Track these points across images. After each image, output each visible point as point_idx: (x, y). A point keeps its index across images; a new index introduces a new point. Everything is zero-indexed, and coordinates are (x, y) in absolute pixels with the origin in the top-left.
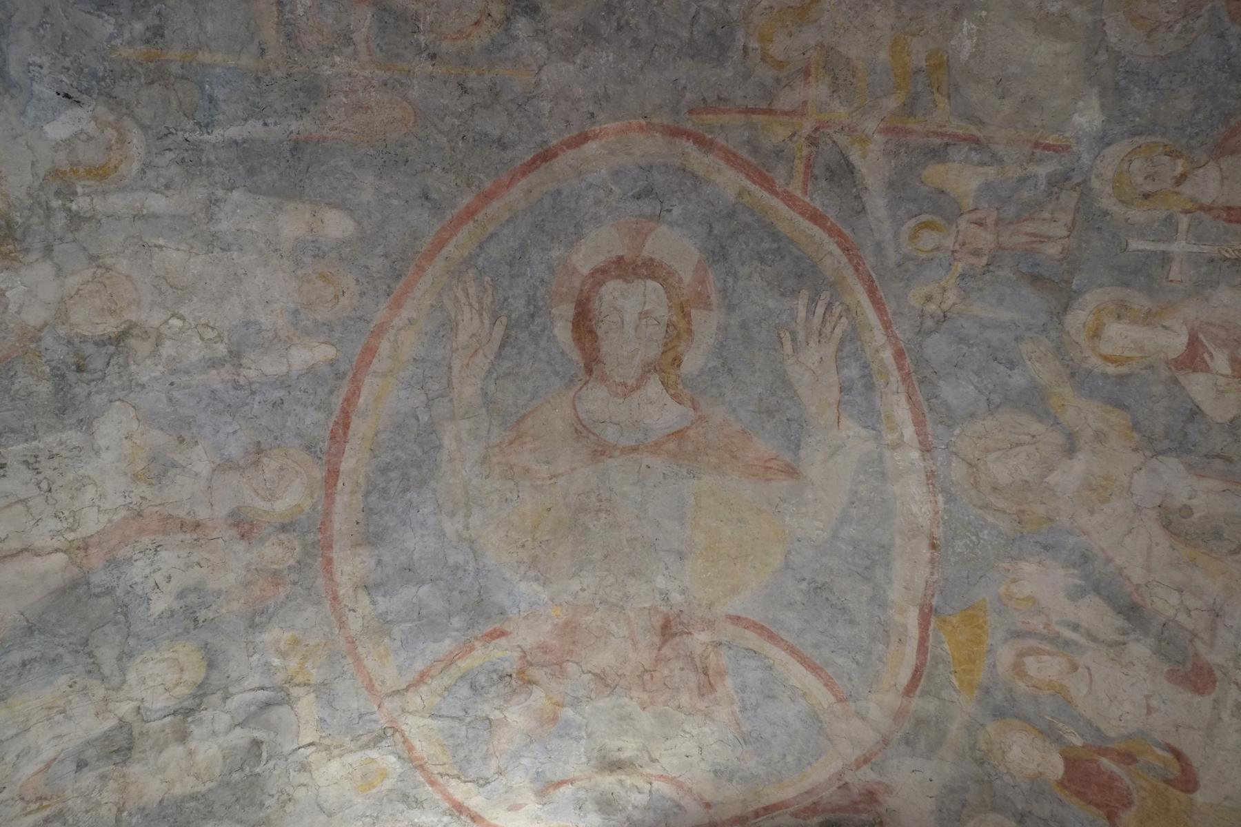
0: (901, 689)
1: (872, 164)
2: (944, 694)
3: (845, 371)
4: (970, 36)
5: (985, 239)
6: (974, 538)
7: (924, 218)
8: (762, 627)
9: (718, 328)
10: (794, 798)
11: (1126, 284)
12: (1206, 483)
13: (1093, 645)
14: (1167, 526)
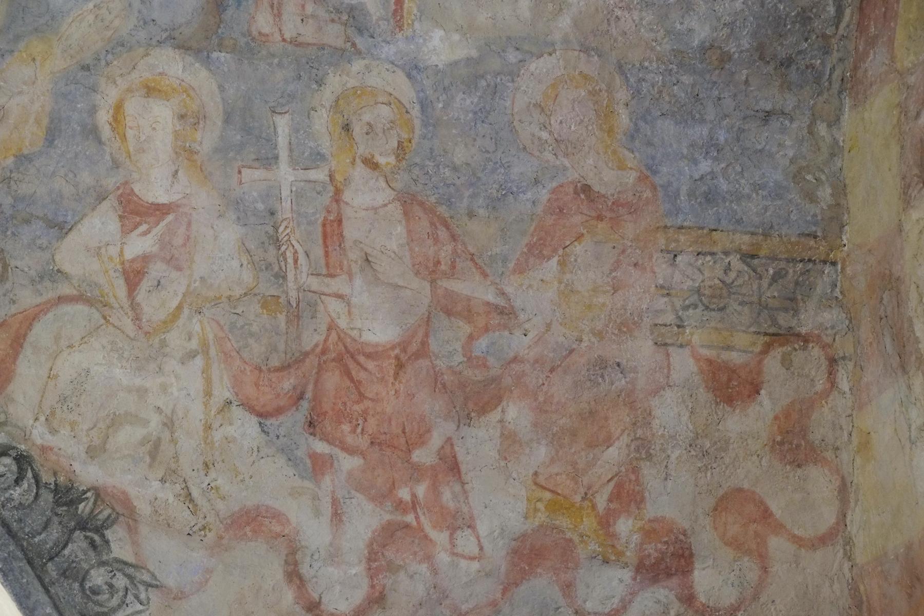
11: (228, 119)
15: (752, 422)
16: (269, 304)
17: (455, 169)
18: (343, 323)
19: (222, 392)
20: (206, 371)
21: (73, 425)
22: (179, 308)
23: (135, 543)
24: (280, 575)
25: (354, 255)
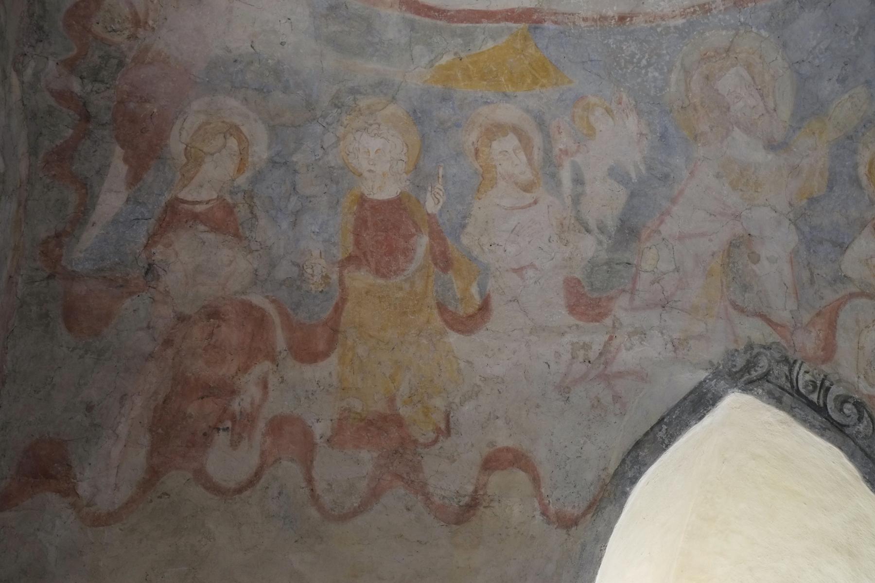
2: (418, 49)
6: (644, 62)
12: (786, 269)
13: (568, 201)
14: (734, 245)
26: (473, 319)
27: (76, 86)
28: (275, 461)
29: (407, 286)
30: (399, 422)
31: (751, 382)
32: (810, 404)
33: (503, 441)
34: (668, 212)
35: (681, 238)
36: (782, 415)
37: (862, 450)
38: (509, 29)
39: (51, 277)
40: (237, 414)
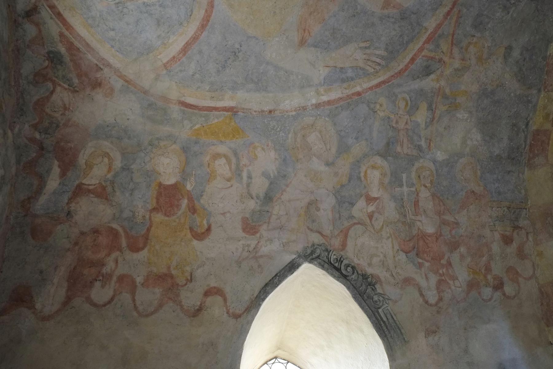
0: (183, 99)
1: (429, 83)
2: (186, 122)
3: (350, 70)
4: (463, 116)
5: (401, 125)
6: (279, 129)
7: (409, 102)
8: (208, 21)
9: (373, 12)
10: (79, 35)
11: (391, 175)
13: (245, 186)
14: (310, 204)
15: (512, 249)
16: (404, 223)
17: (444, 187)
18: (421, 228)
19: (397, 247)
20: (392, 242)
21: (363, 257)
22: (383, 225)
23: (383, 289)
24: (418, 295)
25: (421, 210)
26: (202, 235)
27: (37, 136)
28: (119, 294)
29: (177, 220)
30: (172, 277)
31: (313, 259)
32: (335, 268)
33: (213, 284)
34: (285, 191)
35: (289, 201)
36: (324, 272)
37: (353, 285)
38: (224, 114)
39: (25, 216)
40: (105, 273)
